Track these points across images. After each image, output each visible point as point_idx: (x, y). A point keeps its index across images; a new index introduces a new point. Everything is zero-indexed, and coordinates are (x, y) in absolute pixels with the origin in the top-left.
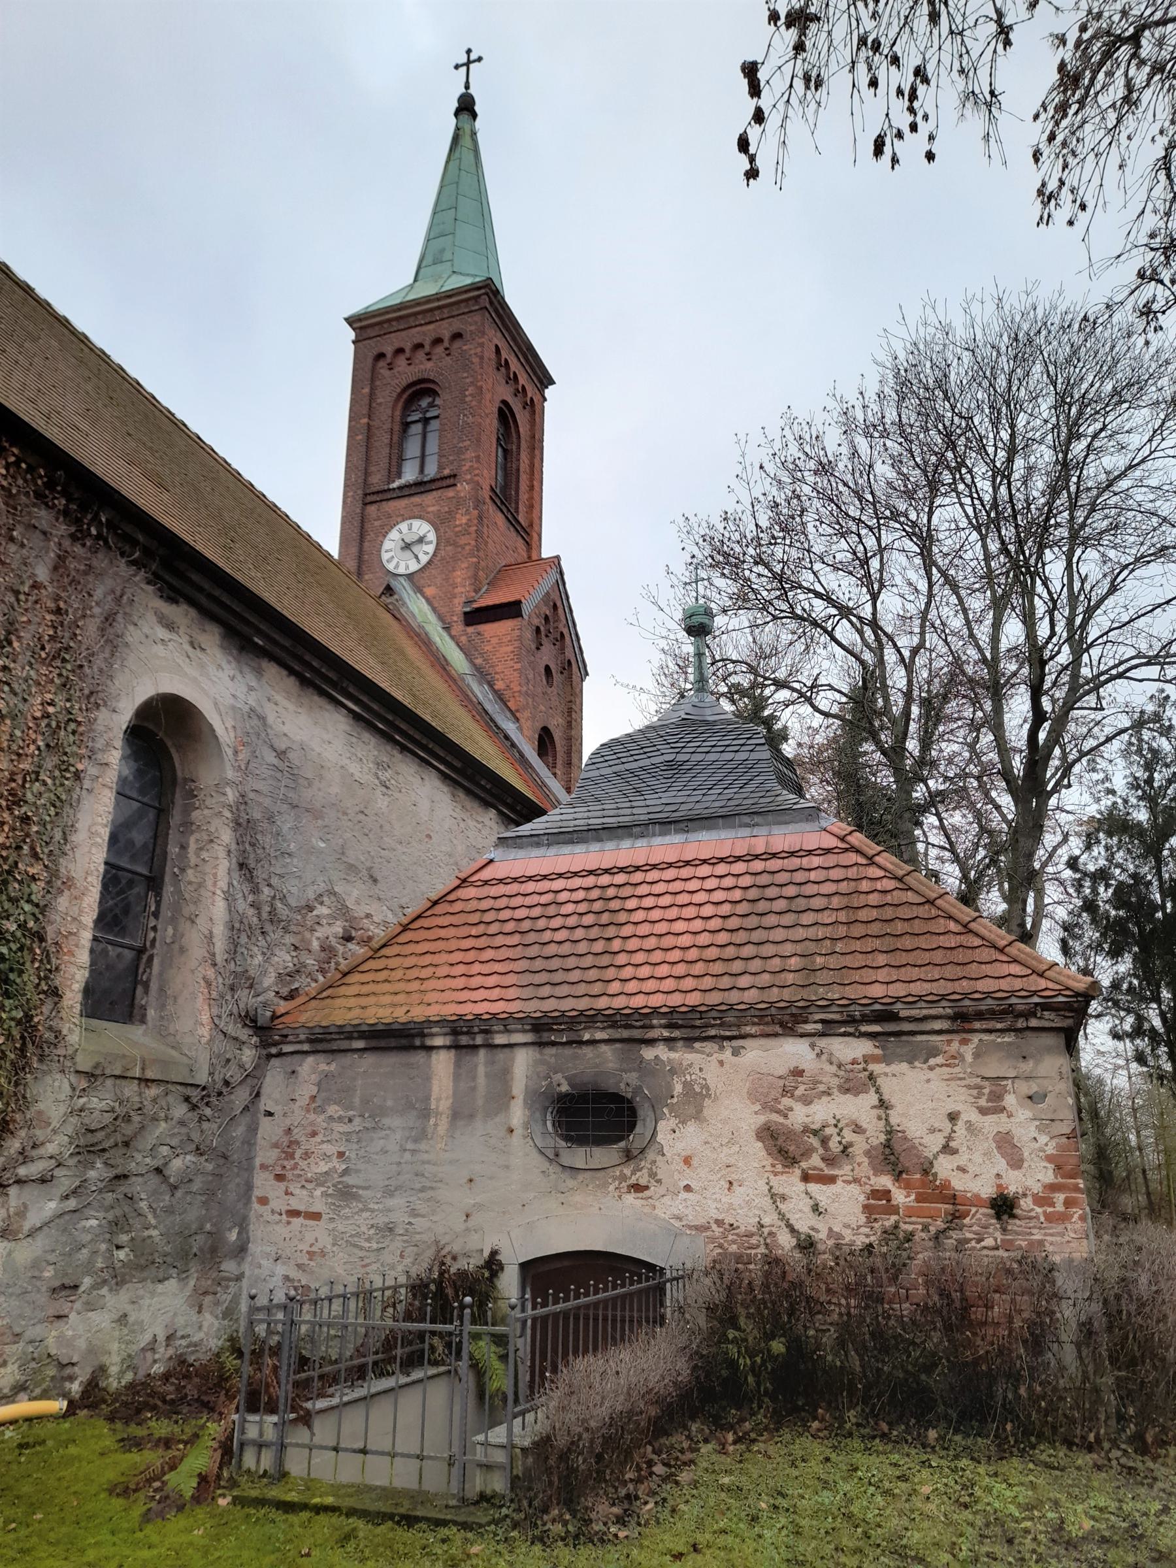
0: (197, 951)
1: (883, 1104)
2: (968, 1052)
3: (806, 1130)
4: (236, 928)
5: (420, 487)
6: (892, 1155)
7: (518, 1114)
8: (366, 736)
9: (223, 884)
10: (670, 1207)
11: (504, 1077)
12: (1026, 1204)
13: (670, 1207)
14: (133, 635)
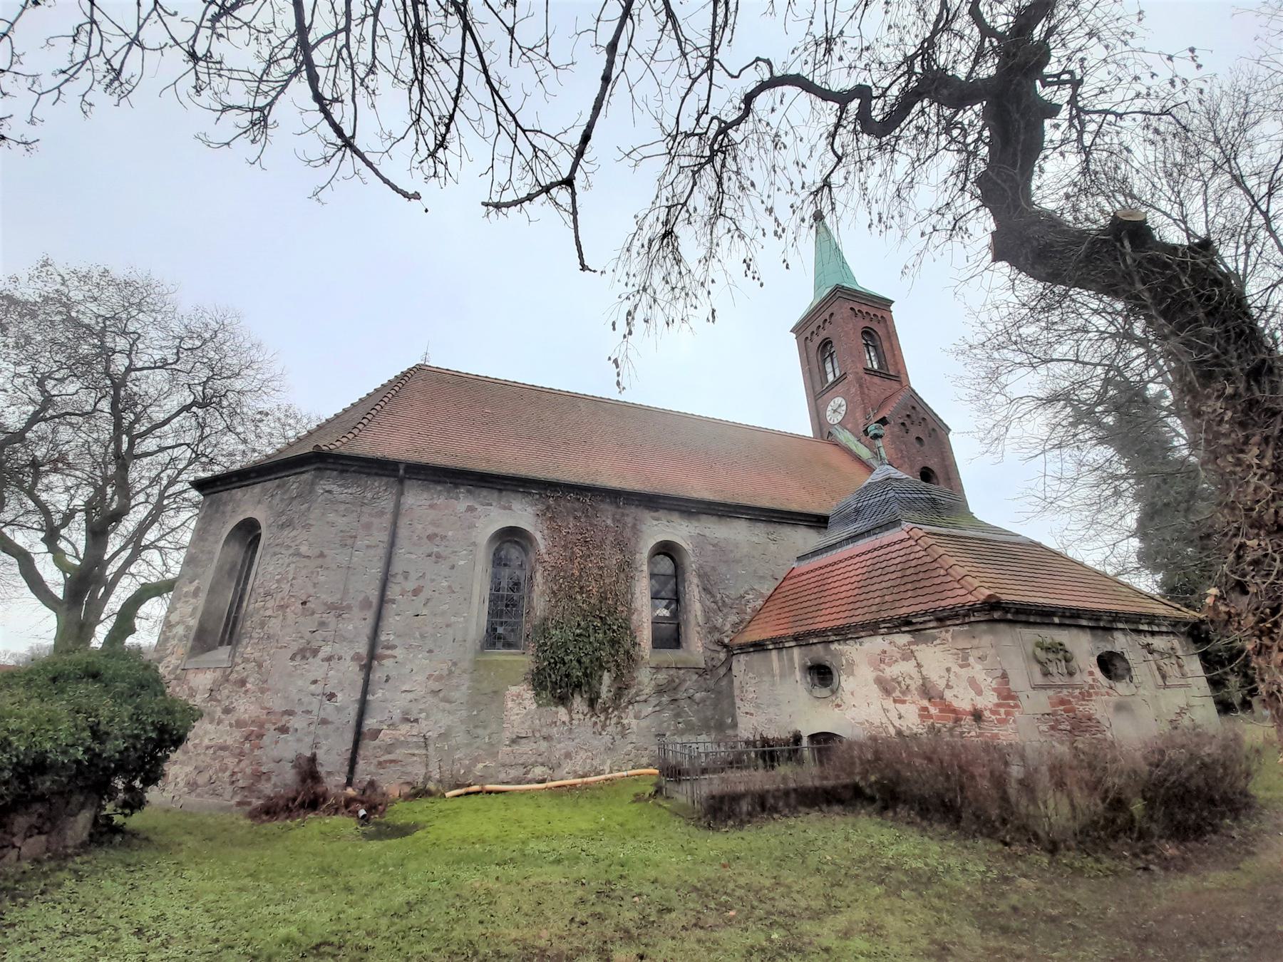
0: (693, 622)
1: (919, 665)
2: (949, 636)
3: (893, 680)
4: (706, 612)
5: (835, 383)
6: (927, 691)
7: (798, 675)
8: (759, 524)
9: (697, 597)
10: (850, 714)
11: (791, 660)
12: (987, 714)
13: (850, 714)
14: (644, 528)
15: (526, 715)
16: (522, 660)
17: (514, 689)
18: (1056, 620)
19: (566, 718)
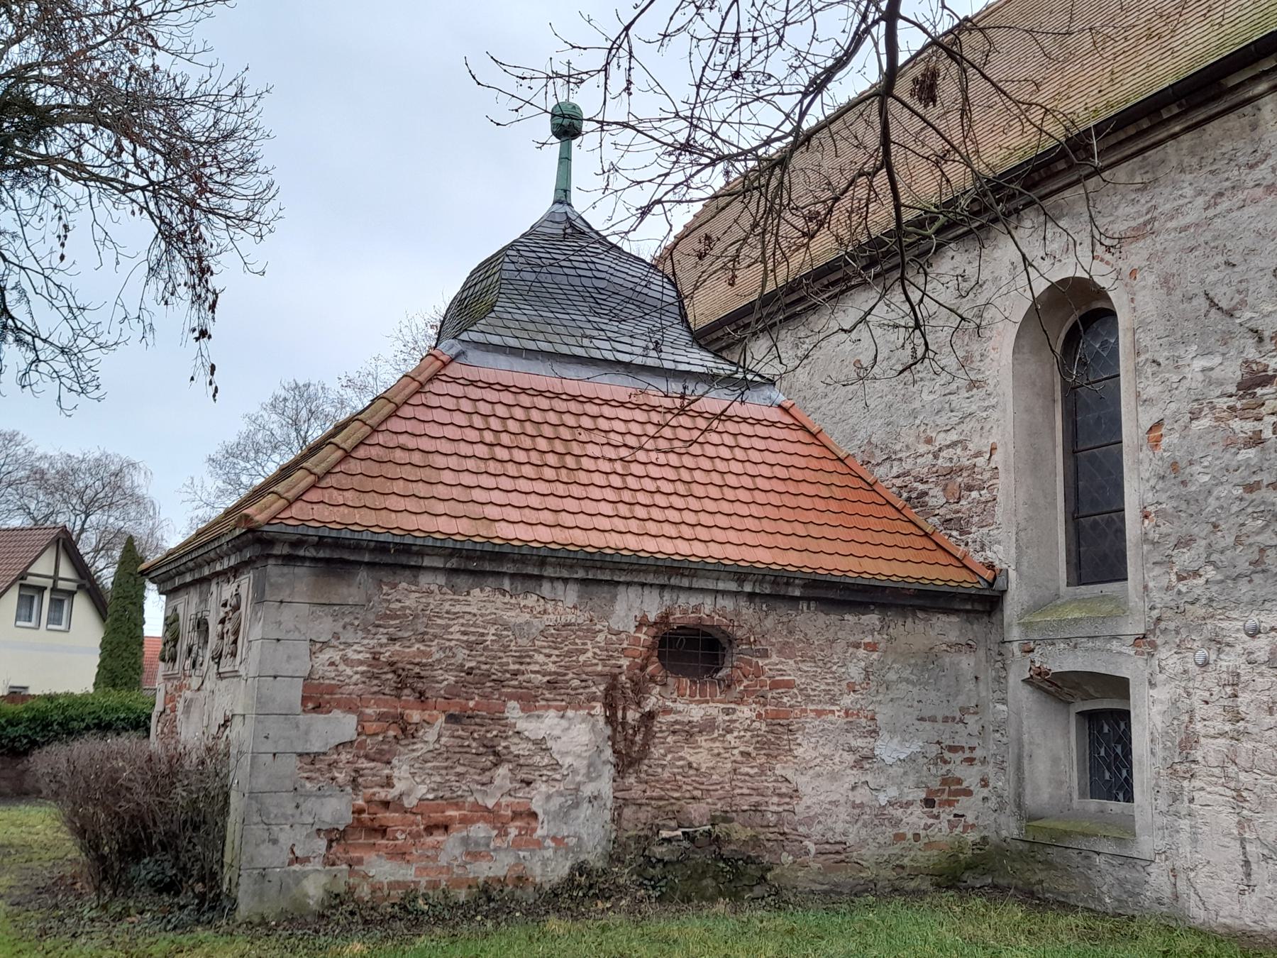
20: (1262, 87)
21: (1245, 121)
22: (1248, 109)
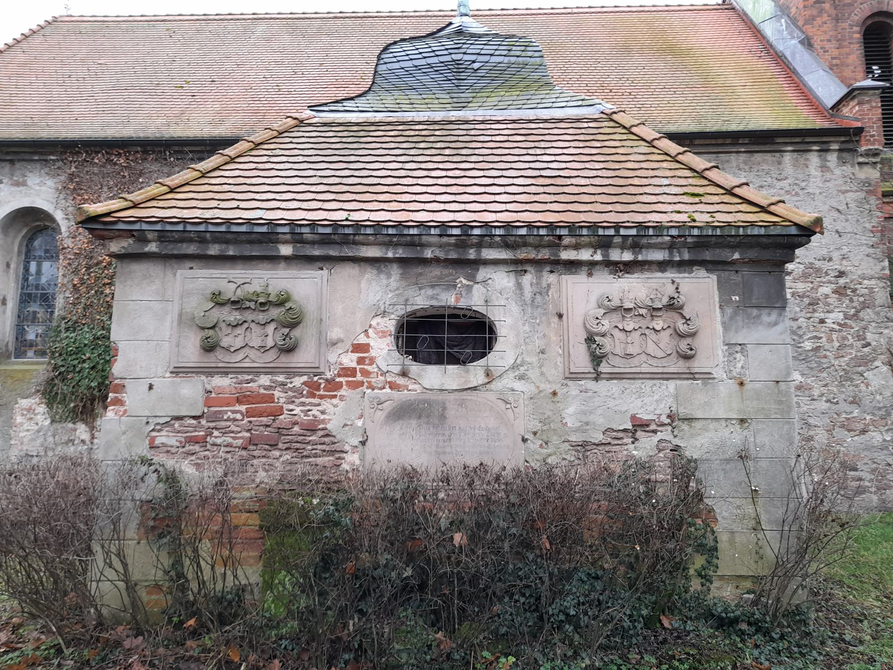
15: (39, 431)
16: (38, 368)
17: (24, 403)
18: (286, 250)
19: (86, 436)
20: (790, 148)
21: (775, 159)
22: (777, 155)
